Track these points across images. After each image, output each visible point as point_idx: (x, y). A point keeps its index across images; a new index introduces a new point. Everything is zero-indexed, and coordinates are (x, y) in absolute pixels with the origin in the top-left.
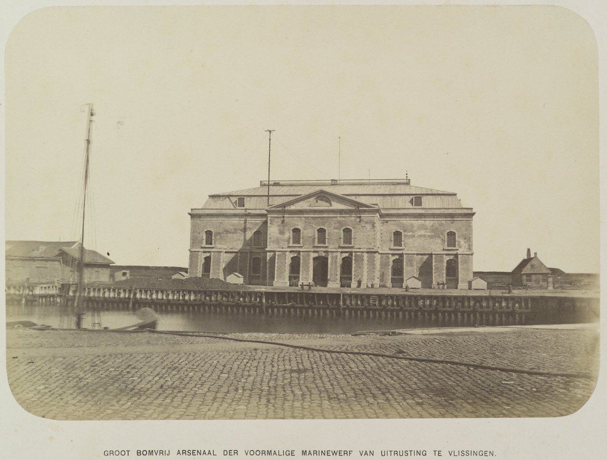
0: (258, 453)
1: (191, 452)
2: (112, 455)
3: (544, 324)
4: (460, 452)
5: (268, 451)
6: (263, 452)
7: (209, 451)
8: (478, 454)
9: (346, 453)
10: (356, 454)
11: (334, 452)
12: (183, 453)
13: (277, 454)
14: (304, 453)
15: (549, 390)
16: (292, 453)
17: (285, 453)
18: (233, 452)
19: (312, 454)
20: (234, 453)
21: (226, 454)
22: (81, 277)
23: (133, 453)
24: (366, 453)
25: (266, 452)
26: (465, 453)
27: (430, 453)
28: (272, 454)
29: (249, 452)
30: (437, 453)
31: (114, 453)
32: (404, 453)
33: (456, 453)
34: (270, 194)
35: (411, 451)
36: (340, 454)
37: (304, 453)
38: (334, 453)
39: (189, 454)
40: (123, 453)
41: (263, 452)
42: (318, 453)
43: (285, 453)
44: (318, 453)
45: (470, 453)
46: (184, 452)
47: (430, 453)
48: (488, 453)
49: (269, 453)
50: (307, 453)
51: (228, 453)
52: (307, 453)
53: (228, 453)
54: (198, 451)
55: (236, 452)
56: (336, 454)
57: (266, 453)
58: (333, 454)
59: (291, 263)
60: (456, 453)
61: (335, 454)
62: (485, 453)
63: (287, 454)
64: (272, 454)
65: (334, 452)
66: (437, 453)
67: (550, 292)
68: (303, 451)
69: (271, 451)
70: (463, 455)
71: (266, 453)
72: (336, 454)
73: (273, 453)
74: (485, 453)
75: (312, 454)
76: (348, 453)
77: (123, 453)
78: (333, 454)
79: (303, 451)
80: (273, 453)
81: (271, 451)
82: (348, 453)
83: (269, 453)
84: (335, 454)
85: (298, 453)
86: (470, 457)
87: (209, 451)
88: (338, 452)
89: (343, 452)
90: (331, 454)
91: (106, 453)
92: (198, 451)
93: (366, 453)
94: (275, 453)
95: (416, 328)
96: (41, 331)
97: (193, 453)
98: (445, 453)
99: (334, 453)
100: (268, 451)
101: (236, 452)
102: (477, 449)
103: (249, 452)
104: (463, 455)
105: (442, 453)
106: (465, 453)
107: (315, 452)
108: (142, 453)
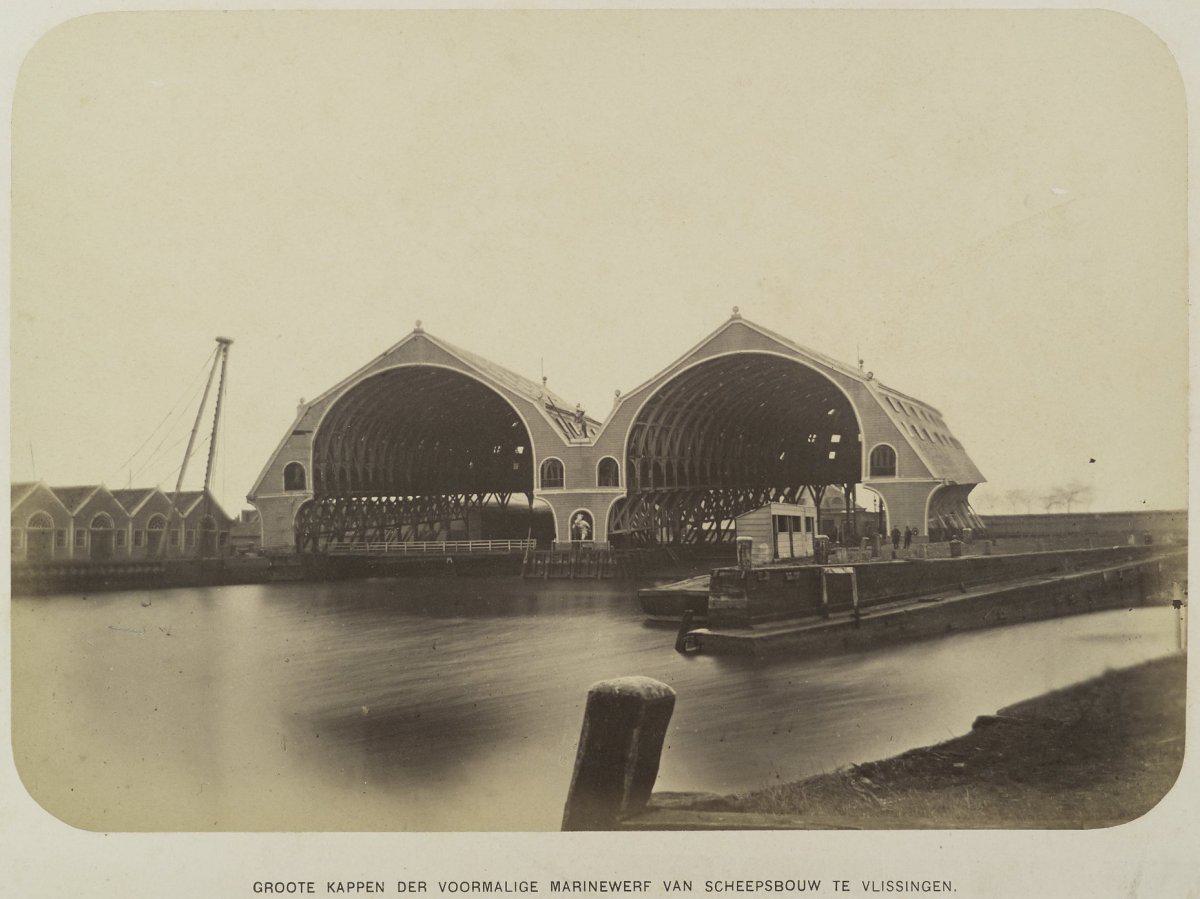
1: (773, 885)
2: (269, 890)
4: (885, 885)
5: (484, 883)
6: (475, 886)
7: (340, 884)
9: (637, 885)
10: (656, 887)
11: (615, 884)
14: (555, 886)
15: (1082, 757)
18: (631, 885)
19: (345, 888)
21: (402, 888)
23: (699, 886)
24: (677, 886)
25: (482, 885)
27: (827, 886)
28: (494, 888)
29: (447, 886)
30: (840, 885)
31: (273, 888)
34: (796, 555)
35: (302, 883)
36: (627, 889)
37: (555, 886)
38: (615, 887)
39: (900, 889)
40: (291, 887)
41: (475, 886)
42: (582, 886)
45: (904, 885)
47: (827, 886)
49: (488, 887)
50: (562, 887)
52: (562, 887)
53: (405, 887)
54: (377, 884)
57: (481, 887)
58: (613, 889)
61: (615, 889)
64: (494, 888)
65: (615, 884)
67: (646, 444)
68: (552, 883)
69: (558, 883)
70: (890, 889)
71: (481, 887)
75: (571, 888)
76: (642, 887)
77: (291, 887)
78: (613, 889)
79: (552, 883)
81: (558, 883)
82: (642, 887)
83: (488, 887)
84: (615, 889)
85: (544, 886)
87: (340, 884)
88: (599, 885)
89: (754, 884)
90: (608, 888)
91: (257, 888)
92: (377, 884)
93: (677, 886)
94: (498, 887)
95: (553, 614)
98: (855, 886)
99: (615, 887)
100: (484, 883)
101: (423, 886)
103: (447, 886)
104: (890, 889)
105: (850, 886)
106: (895, 887)
107: (577, 885)
108: (784, 886)
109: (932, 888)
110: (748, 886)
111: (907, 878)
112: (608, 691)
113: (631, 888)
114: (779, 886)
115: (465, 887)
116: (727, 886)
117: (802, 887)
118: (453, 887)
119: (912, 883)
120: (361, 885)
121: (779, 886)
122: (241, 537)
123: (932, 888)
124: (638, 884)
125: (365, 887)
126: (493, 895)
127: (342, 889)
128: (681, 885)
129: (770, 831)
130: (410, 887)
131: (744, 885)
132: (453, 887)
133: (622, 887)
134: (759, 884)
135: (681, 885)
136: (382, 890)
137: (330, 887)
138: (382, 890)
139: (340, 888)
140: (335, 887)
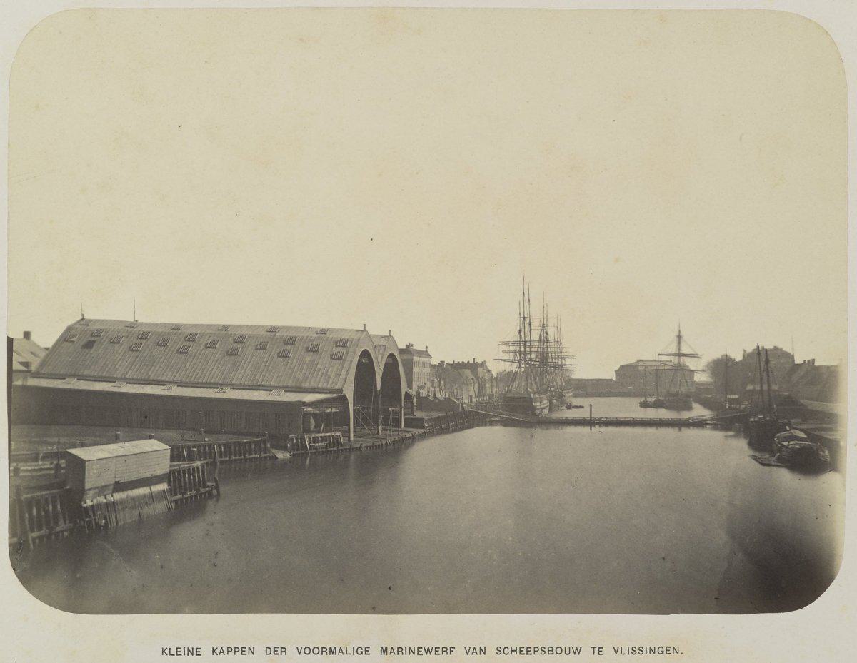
0: (506, 651)
1: (546, 650)
2: (445, 653)
3: (201, 399)
6: (324, 650)
8: (656, 652)
9: (445, 650)
11: (577, 649)
12: (398, 651)
13: (344, 651)
16: (366, 651)
17: (355, 650)
18: (440, 650)
19: (396, 652)
20: (443, 651)
21: (268, 652)
22: (679, 360)
25: (328, 650)
26: (638, 651)
28: (389, 652)
30: (596, 650)
32: (630, 651)
33: (625, 651)
36: (243, 653)
38: (428, 651)
42: (404, 651)
43: (355, 650)
44: (404, 652)
45: (644, 650)
46: (445, 649)
48: (671, 649)
51: (273, 651)
53: (273, 651)
55: (284, 650)
56: (431, 653)
58: (426, 653)
59: (718, 359)
60: (625, 651)
62: (666, 651)
63: (359, 653)
64: (389, 652)
65: (577, 649)
66: (596, 650)
72: (431, 653)
73: (389, 650)
74: (666, 651)
75: (396, 652)
76: (449, 651)
77: (316, 651)
78: (426, 653)
80: (389, 650)
82: (449, 651)
86: (555, 658)
90: (423, 652)
92: (249, 648)
93: (474, 651)
96: (159, 379)
97: (366, 651)
100: (330, 648)
101: (284, 650)
102: (432, 644)
103: (656, 650)
105: (604, 651)
106: (638, 651)
108: (554, 651)
109: (364, 653)
110: (527, 651)
111: (646, 644)
112: (725, 357)
113: (279, 652)
114: (551, 651)
115: (316, 651)
116: (516, 651)
117: (568, 652)
118: (307, 651)
119: (188, 649)
120: (237, 650)
121: (551, 651)
122: (768, 375)
123: (364, 653)
124: (445, 649)
125: (233, 651)
126: (333, 658)
127: (223, 652)
128: (478, 650)
129: (7, 457)
130: (275, 651)
131: (525, 650)
132: (307, 651)
133: (416, 653)
134: (536, 649)
135: (478, 650)
136: (253, 653)
137: (163, 651)
138: (253, 653)
139: (222, 651)
140: (218, 651)
